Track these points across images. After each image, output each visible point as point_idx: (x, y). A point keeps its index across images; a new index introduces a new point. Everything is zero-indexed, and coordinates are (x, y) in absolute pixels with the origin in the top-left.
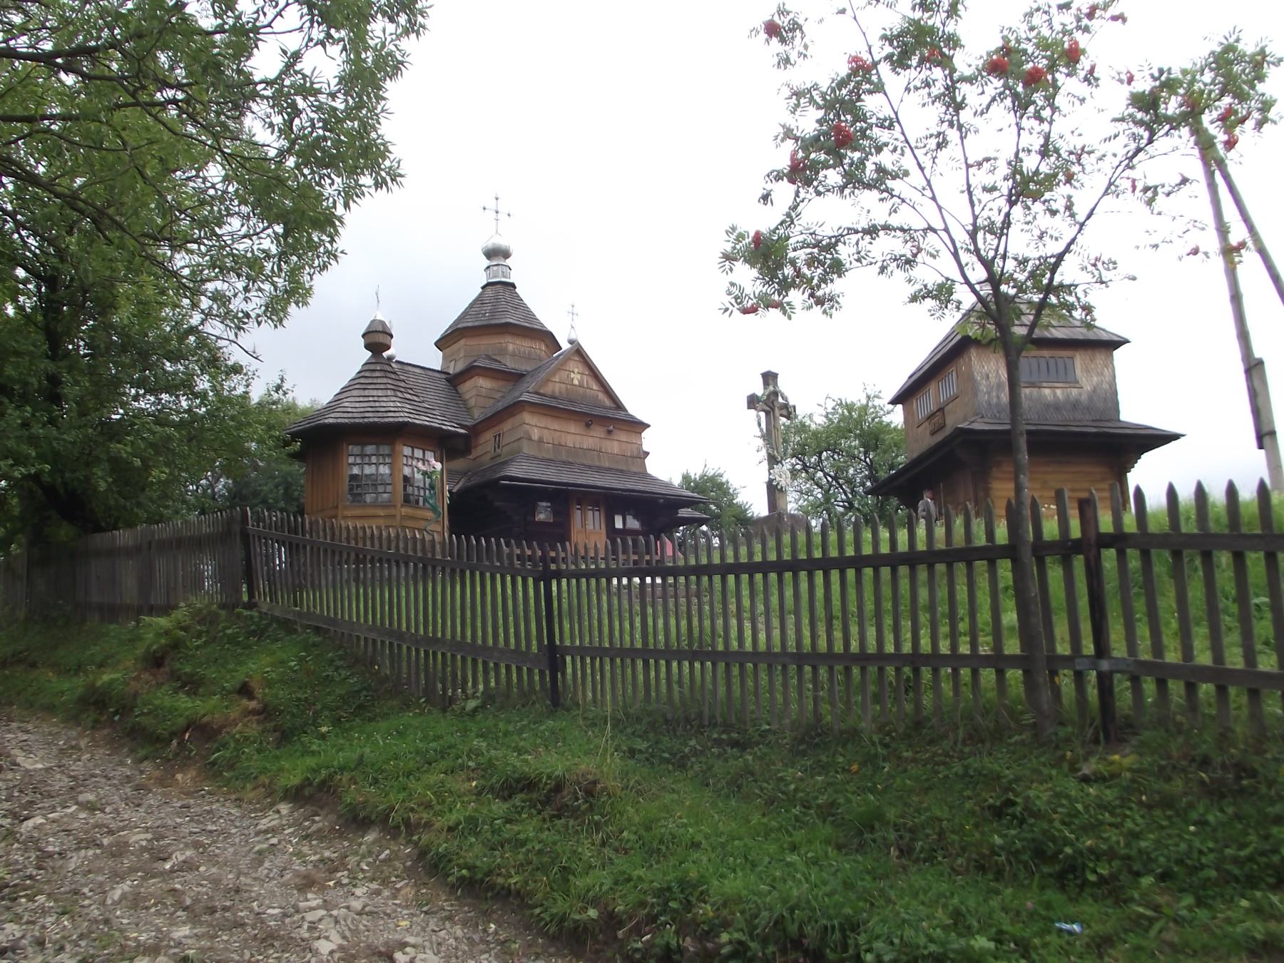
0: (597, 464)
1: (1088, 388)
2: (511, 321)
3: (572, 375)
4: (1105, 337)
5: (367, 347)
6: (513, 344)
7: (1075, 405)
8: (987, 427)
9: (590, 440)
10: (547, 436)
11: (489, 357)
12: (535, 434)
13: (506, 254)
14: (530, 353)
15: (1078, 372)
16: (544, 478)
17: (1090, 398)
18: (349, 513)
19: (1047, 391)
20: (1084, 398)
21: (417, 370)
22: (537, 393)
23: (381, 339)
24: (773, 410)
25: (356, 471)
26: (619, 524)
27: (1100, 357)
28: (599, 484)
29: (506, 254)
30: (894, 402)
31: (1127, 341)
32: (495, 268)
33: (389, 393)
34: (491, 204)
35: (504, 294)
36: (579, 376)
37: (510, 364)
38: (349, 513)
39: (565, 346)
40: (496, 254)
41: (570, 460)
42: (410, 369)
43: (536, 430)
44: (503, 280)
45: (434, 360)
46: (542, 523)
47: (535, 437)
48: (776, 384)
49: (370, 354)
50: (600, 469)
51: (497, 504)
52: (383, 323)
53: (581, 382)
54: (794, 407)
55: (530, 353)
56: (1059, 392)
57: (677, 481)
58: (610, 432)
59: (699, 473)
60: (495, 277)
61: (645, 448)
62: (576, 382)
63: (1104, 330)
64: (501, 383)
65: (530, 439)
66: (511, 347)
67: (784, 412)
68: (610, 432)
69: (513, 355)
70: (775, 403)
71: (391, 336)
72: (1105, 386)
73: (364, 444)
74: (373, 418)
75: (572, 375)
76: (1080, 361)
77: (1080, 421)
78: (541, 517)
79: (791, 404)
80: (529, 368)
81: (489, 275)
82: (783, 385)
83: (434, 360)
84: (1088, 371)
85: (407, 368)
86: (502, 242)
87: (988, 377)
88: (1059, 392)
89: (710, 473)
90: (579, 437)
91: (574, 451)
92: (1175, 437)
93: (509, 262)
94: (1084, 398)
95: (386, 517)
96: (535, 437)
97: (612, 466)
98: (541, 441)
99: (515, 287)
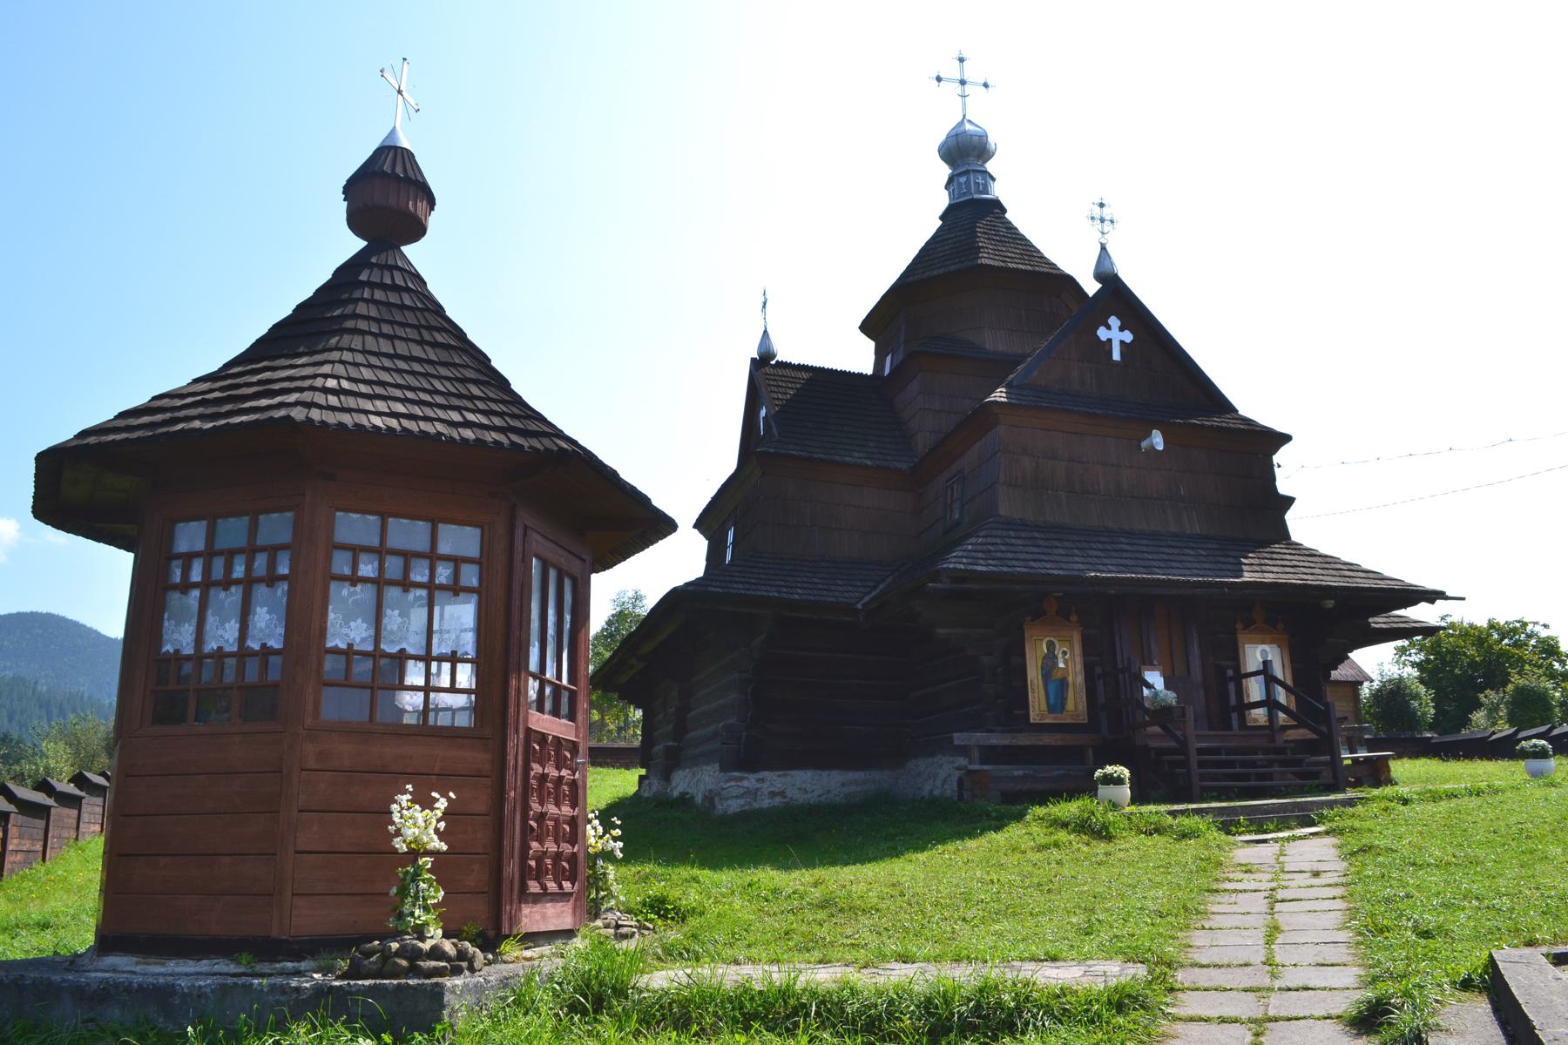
5: (356, 222)
32: (963, 179)
34: (952, 71)
39: (1091, 287)
45: (859, 357)
49: (358, 244)
52: (406, 156)
57: (1502, 623)
61: (1283, 487)
71: (431, 202)
83: (859, 357)
99: (1004, 210)
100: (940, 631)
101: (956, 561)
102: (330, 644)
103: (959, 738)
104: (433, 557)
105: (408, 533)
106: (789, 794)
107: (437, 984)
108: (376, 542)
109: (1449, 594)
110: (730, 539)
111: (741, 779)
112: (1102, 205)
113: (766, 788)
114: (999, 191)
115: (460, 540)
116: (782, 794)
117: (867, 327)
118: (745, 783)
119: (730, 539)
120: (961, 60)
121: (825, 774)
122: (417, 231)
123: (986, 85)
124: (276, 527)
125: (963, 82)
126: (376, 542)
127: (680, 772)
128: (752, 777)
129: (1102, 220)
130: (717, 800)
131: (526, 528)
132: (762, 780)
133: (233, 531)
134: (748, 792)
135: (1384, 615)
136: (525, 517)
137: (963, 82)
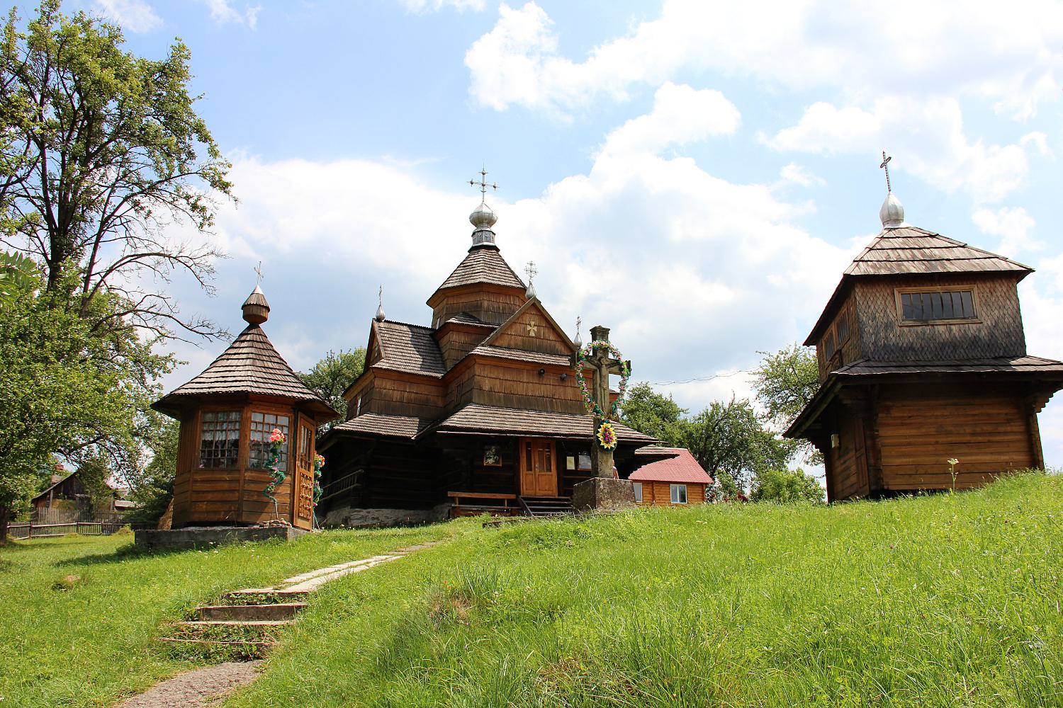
1: (989, 322)
2: (485, 280)
3: (529, 328)
5: (245, 317)
6: (486, 302)
7: (975, 342)
13: (491, 221)
15: (977, 307)
16: (482, 426)
17: (992, 335)
18: (198, 477)
19: (942, 329)
20: (983, 333)
21: (405, 328)
23: (255, 311)
25: (208, 437)
26: (570, 464)
27: (1001, 288)
29: (491, 221)
30: (807, 343)
31: (1030, 271)
32: (480, 234)
33: (248, 362)
34: (478, 179)
36: (535, 328)
42: (398, 327)
46: (489, 467)
47: (486, 388)
51: (445, 450)
53: (537, 333)
54: (628, 363)
58: (562, 379)
60: (480, 242)
62: (532, 334)
65: (481, 389)
66: (486, 304)
67: (615, 369)
68: (562, 379)
69: (488, 310)
70: (604, 361)
72: (1008, 320)
73: (228, 412)
74: (220, 388)
75: (529, 328)
76: (977, 293)
77: (979, 359)
78: (491, 461)
79: (623, 360)
81: (474, 242)
82: (614, 340)
84: (987, 304)
85: (393, 326)
89: (738, 401)
92: (677, 455)
93: (493, 228)
94: (983, 333)
95: (230, 481)
96: (486, 388)
99: (498, 250)
100: (445, 450)
101: (455, 420)
102: (574, 468)
103: (450, 494)
104: (263, 423)
105: (270, 419)
106: (380, 518)
107: (429, 369)
108: (262, 421)
109: (733, 398)
110: (359, 404)
111: (360, 511)
112: (531, 264)
113: (370, 516)
114: (497, 242)
115: (284, 420)
116: (378, 519)
117: (430, 303)
118: (361, 513)
119: (359, 404)
120: (483, 174)
121: (397, 510)
122: (265, 319)
123: (495, 187)
124: (233, 416)
125: (483, 185)
126: (262, 421)
127: (331, 513)
128: (365, 511)
129: (531, 272)
130: (349, 520)
131: (301, 417)
132: (369, 512)
133: (221, 417)
134: (362, 517)
135: (987, 450)
136: (300, 414)
137: (483, 185)
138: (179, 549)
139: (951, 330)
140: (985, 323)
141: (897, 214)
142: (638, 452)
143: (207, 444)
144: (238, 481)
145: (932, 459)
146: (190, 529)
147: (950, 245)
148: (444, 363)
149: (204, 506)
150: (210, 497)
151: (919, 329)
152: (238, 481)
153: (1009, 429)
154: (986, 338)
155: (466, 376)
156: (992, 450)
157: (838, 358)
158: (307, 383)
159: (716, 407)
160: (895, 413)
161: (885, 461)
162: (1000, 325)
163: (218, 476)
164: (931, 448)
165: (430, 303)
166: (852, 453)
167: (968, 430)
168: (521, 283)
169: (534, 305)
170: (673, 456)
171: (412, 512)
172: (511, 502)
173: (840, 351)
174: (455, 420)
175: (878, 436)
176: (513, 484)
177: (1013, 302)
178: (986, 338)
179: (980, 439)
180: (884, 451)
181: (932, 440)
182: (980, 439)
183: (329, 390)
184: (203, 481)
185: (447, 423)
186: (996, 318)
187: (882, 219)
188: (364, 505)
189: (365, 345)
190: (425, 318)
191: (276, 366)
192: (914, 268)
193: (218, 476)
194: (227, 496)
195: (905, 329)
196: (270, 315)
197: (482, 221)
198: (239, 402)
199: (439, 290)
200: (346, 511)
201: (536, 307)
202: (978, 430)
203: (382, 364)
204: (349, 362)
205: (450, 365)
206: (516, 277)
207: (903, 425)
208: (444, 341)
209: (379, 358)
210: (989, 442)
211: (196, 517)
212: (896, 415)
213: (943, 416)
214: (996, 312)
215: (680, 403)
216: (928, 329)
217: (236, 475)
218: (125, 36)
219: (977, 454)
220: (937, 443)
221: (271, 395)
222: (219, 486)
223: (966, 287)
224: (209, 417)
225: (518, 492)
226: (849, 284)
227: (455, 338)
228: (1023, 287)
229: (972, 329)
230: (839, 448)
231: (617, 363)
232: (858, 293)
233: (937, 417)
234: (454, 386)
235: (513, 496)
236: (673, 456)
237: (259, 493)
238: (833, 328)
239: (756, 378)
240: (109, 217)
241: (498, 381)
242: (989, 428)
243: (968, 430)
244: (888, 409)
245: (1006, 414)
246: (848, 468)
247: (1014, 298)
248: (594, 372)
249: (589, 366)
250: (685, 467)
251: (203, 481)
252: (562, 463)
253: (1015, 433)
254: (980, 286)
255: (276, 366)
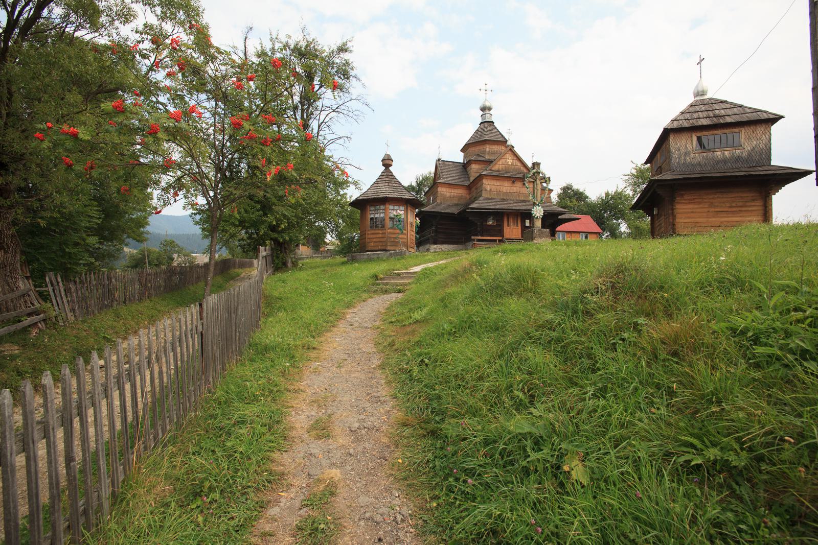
0: (518, 198)
1: (748, 147)
4: (765, 116)
5: (383, 165)
6: (488, 148)
7: (738, 159)
8: (677, 177)
9: (515, 188)
10: (494, 188)
11: (478, 155)
12: (488, 188)
14: (497, 151)
15: (742, 140)
16: (487, 207)
17: (749, 154)
18: (369, 233)
21: (451, 163)
22: (490, 170)
23: (387, 162)
24: (536, 181)
25: (372, 216)
27: (760, 129)
28: (513, 208)
29: (490, 109)
31: (782, 117)
33: (386, 184)
34: (484, 88)
35: (487, 126)
37: (488, 157)
38: (369, 233)
40: (484, 109)
41: (505, 198)
42: (447, 163)
43: (488, 186)
44: (487, 120)
46: (490, 225)
48: (539, 168)
49: (384, 168)
50: (518, 201)
52: (389, 156)
54: (549, 178)
55: (497, 151)
56: (726, 153)
59: (614, 191)
62: (510, 163)
63: (766, 112)
64: (483, 166)
65: (486, 190)
66: (488, 150)
67: (543, 181)
76: (744, 133)
78: (490, 223)
79: (547, 176)
80: (493, 158)
84: (749, 138)
85: (445, 163)
86: (487, 104)
87: (679, 150)
88: (726, 153)
90: (509, 188)
91: (506, 194)
93: (491, 112)
96: (489, 189)
97: (525, 199)
98: (491, 190)
99: (493, 123)
103: (473, 237)
115: (402, 208)
117: (462, 150)
122: (391, 165)
124: (382, 207)
127: (2, 459)
138: (770, 153)
139: (724, 154)
140: (746, 149)
141: (703, 91)
142: (560, 217)
143: (372, 219)
144: (385, 233)
145: (705, 220)
146: (368, 253)
147: (732, 106)
148: (469, 179)
149: (372, 244)
150: (374, 240)
151: (705, 154)
152: (385, 233)
153: (753, 204)
154: (746, 157)
155: (479, 185)
156: (741, 215)
157: (660, 170)
158: (411, 188)
159: (607, 194)
160: (686, 197)
161: (677, 220)
162: (756, 149)
163: (377, 232)
164: (705, 214)
165: (462, 150)
166: (663, 217)
167: (728, 205)
168: (505, 139)
169: (510, 149)
170: (578, 219)
171: (454, 246)
172: (500, 241)
173: (660, 167)
174: (474, 205)
175: (675, 209)
176: (500, 232)
177: (767, 136)
178: (746, 157)
179: (734, 209)
180: (678, 216)
181: (706, 210)
182: (734, 209)
183: (418, 192)
184: (371, 234)
185: (471, 206)
186: (754, 146)
187: (694, 95)
188: (435, 243)
189: (433, 170)
190: (460, 158)
191: (397, 185)
192: (705, 122)
193: (377, 232)
194: (382, 240)
195: (696, 154)
196: (393, 164)
197: (387, 162)
198: (384, 201)
199: (466, 145)
200: (427, 246)
201: (511, 149)
202: (734, 205)
203: (441, 181)
204: (426, 179)
205: (472, 180)
206: (502, 136)
207: (689, 203)
208: (468, 169)
209: (440, 178)
210: (740, 211)
211: (370, 248)
212: (687, 198)
213: (713, 198)
214: (755, 142)
215: (587, 193)
216: (710, 154)
217: (384, 231)
218: (354, 87)
219: (732, 217)
220: (708, 211)
221: (394, 198)
222: (378, 236)
223: (737, 130)
224: (372, 209)
225: (503, 236)
226: (667, 133)
227: (474, 167)
228: (775, 128)
229: (738, 152)
230: (658, 214)
231: (544, 178)
232: (673, 140)
233: (710, 199)
234: (473, 189)
235: (501, 238)
236: (578, 219)
237: (395, 238)
238: (659, 155)
239: (627, 178)
240: (322, 123)
241: (700, 113)
242: (741, 204)
243: (728, 205)
244: (682, 195)
245: (752, 196)
246: (661, 224)
247: (768, 133)
248: (533, 182)
249: (531, 180)
250: (587, 223)
251: (371, 234)
252: (523, 223)
253: (758, 206)
254: (746, 128)
255: (397, 185)
